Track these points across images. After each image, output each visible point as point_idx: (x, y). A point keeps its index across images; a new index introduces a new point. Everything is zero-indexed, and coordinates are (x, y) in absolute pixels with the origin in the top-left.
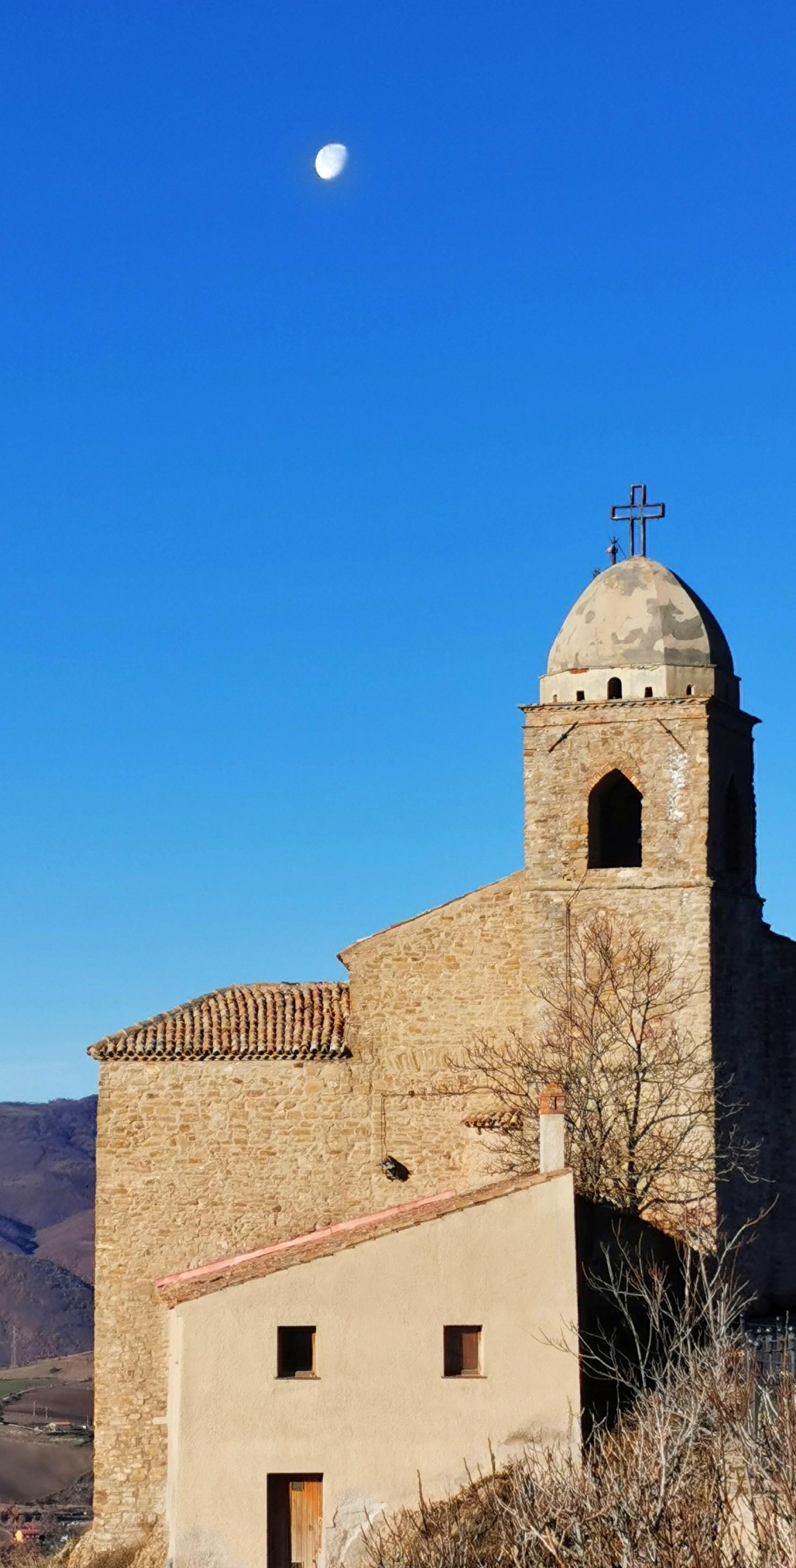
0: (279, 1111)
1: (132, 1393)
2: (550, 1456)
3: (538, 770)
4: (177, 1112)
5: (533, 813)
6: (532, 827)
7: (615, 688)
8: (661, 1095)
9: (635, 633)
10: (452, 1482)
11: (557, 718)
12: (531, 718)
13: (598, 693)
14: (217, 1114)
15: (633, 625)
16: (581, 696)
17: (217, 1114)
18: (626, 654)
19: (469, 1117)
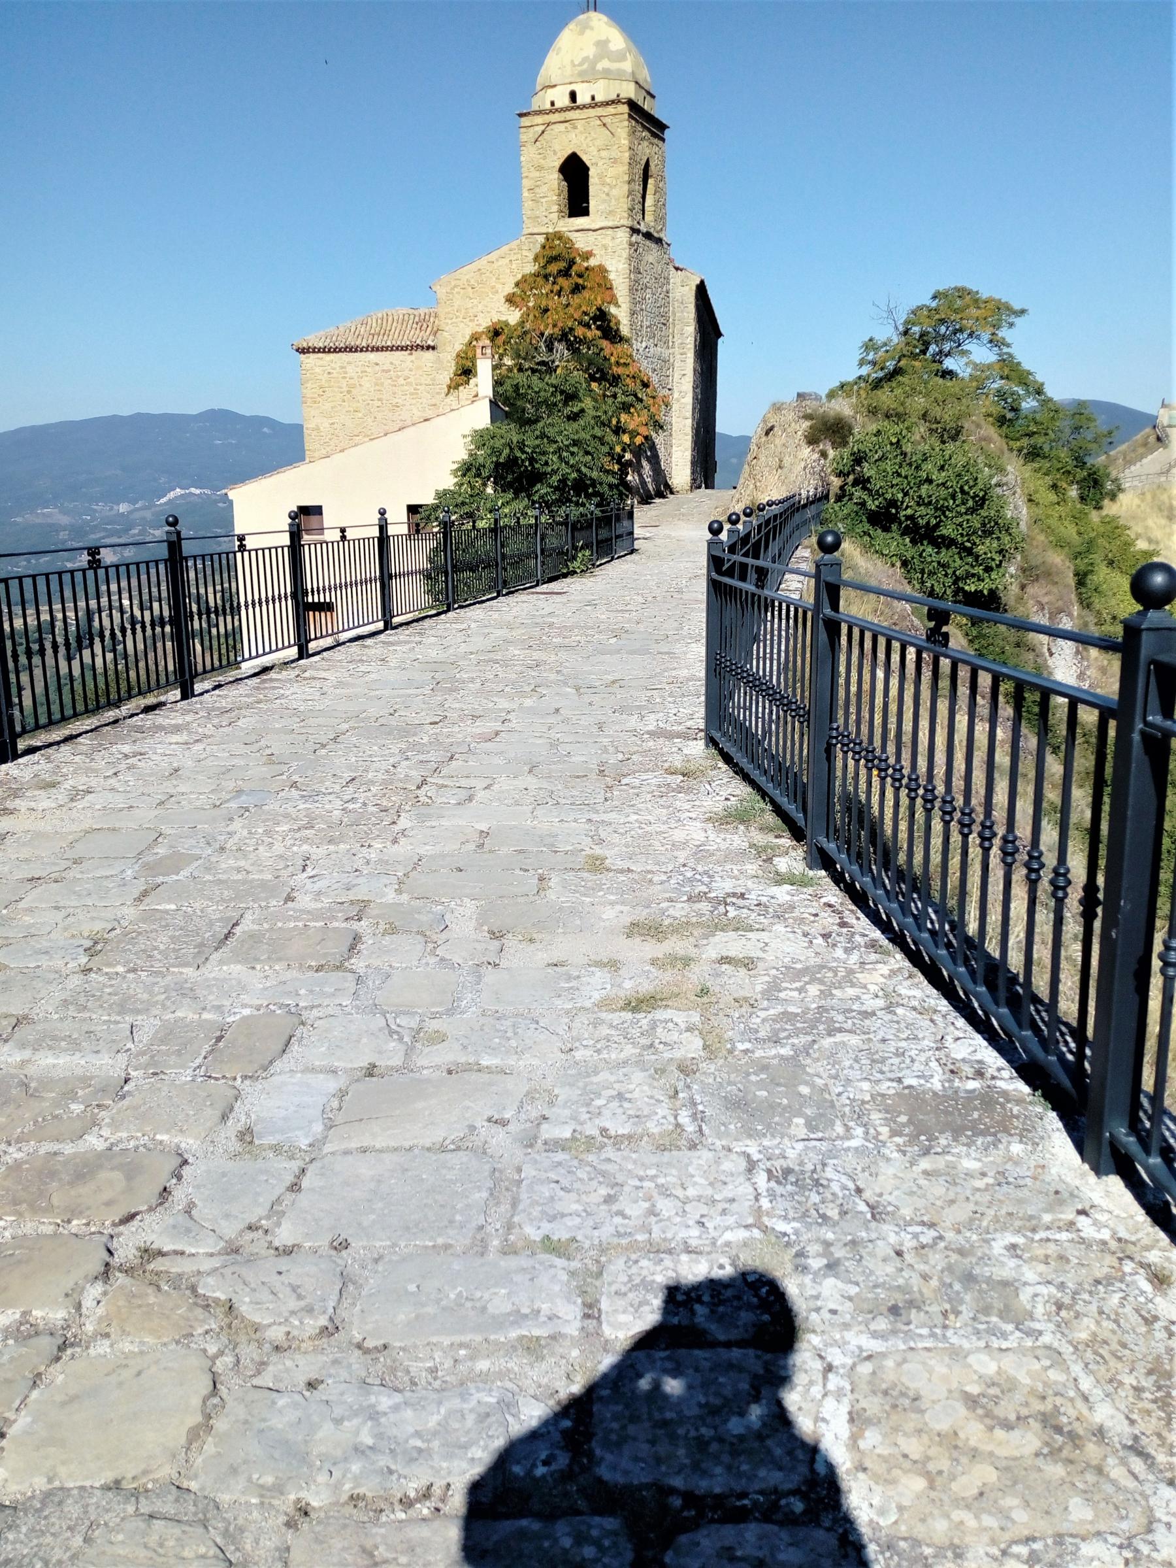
0: (401, 381)
1: (58, 1106)
2: (767, 434)
3: (528, 155)
4: (344, 384)
5: (526, 183)
6: (526, 194)
7: (573, 96)
8: (805, 716)
9: (585, 59)
10: (678, 1103)
11: (539, 119)
12: (525, 121)
13: (564, 101)
14: (367, 383)
15: (584, 54)
16: (553, 104)
17: (367, 383)
18: (581, 74)
19: (587, 256)
